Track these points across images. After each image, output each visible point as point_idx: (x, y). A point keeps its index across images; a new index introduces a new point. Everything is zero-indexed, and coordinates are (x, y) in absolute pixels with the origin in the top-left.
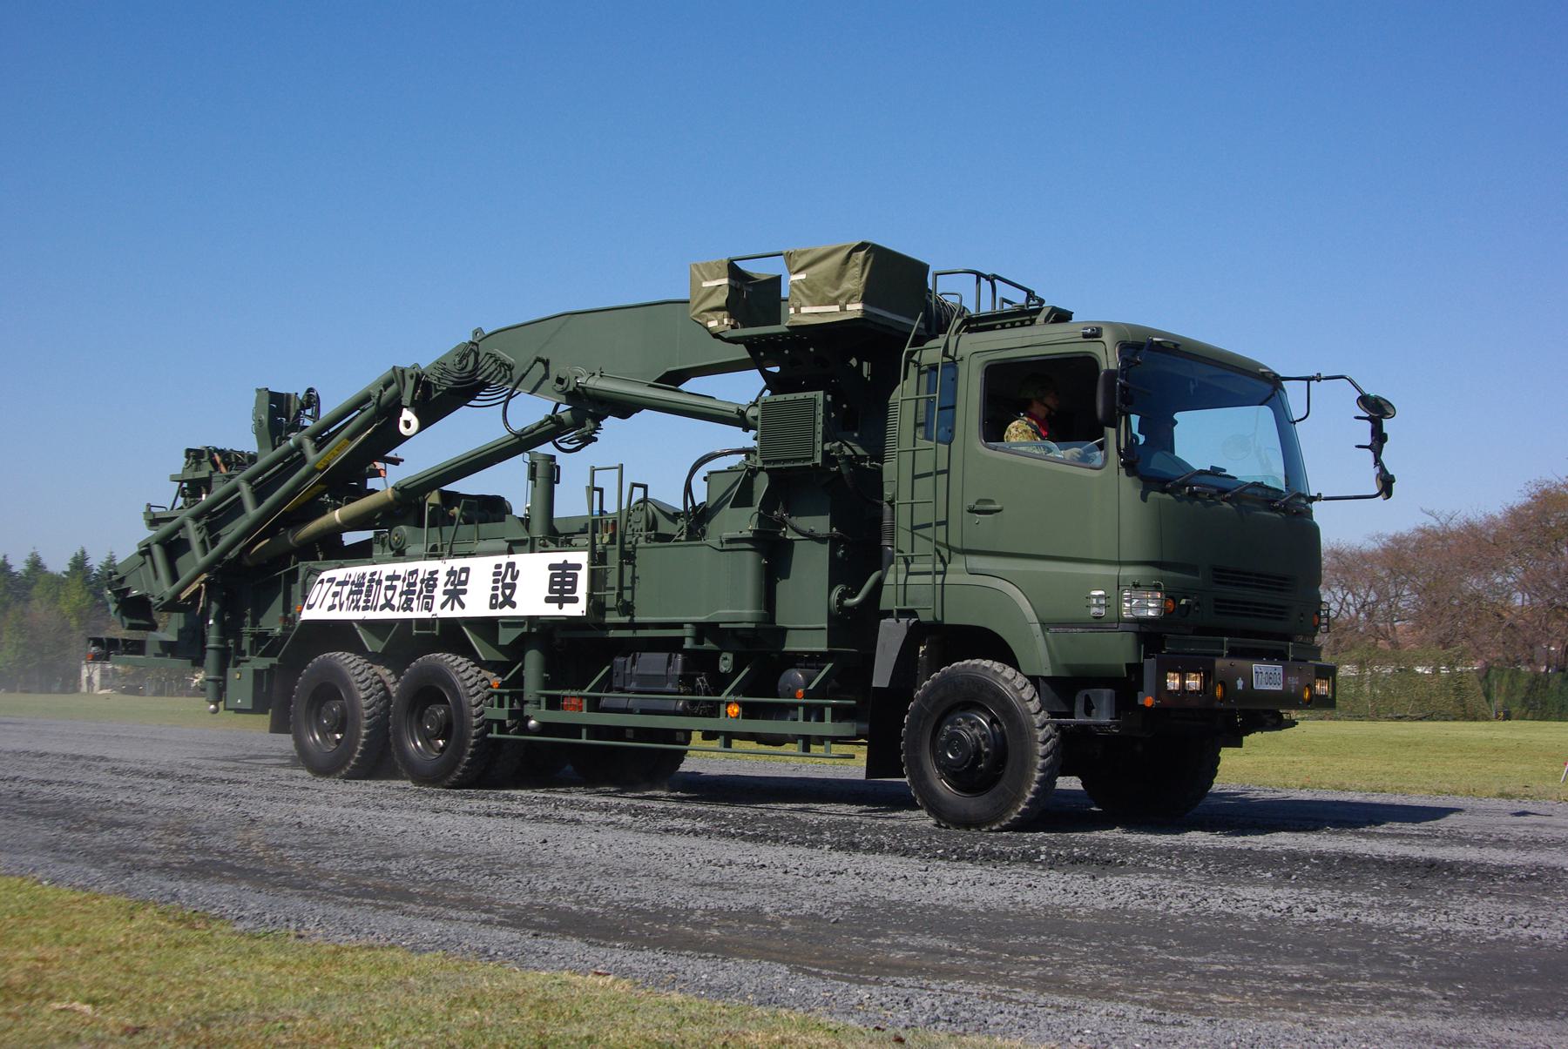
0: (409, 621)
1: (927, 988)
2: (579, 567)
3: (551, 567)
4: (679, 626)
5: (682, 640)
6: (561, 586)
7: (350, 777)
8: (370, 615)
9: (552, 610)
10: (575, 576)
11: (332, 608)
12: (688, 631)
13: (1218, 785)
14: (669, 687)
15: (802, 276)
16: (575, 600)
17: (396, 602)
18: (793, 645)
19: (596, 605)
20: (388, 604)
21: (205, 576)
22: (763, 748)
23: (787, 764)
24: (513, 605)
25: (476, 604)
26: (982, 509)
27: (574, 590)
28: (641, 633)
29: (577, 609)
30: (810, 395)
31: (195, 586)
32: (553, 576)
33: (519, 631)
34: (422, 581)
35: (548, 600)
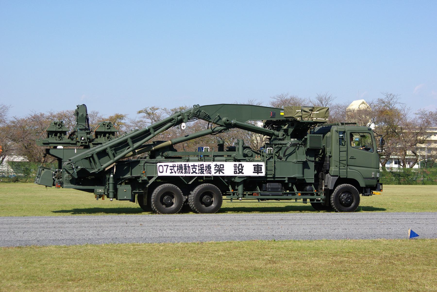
0: (203, 176)
1: (168, 264)
2: (262, 166)
3: (254, 165)
4: (285, 178)
5: (285, 181)
6: (257, 169)
7: (179, 213)
8: (187, 175)
9: (256, 175)
10: (261, 168)
11: (171, 173)
12: (286, 179)
13: (222, 207)
14: (279, 190)
15: (318, 112)
16: (262, 173)
17: (197, 171)
18: (308, 181)
19: (266, 174)
20: (194, 172)
21: (115, 164)
22: (277, 201)
23: (292, 203)
24: (243, 173)
25: (213, 173)
26: (352, 158)
27: (261, 170)
28: (276, 179)
29: (263, 174)
30: (320, 135)
31: (112, 166)
32: (254, 167)
33: (243, 179)
34: (206, 167)
35: (254, 172)
